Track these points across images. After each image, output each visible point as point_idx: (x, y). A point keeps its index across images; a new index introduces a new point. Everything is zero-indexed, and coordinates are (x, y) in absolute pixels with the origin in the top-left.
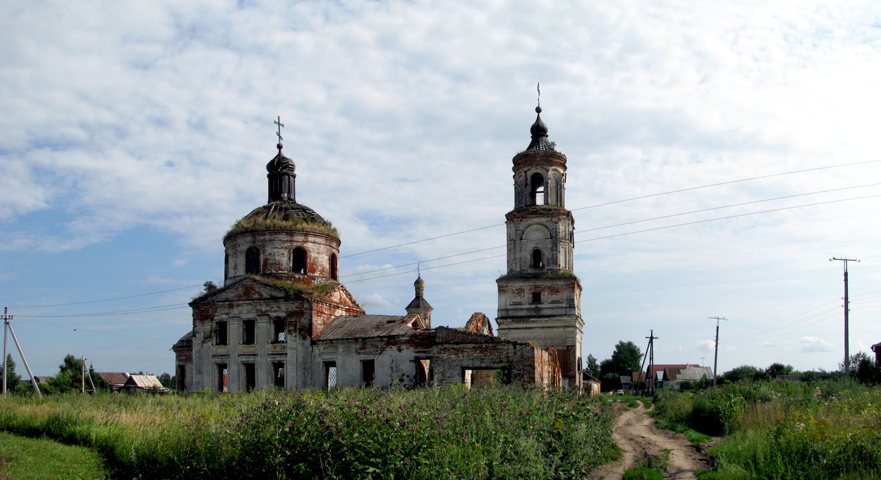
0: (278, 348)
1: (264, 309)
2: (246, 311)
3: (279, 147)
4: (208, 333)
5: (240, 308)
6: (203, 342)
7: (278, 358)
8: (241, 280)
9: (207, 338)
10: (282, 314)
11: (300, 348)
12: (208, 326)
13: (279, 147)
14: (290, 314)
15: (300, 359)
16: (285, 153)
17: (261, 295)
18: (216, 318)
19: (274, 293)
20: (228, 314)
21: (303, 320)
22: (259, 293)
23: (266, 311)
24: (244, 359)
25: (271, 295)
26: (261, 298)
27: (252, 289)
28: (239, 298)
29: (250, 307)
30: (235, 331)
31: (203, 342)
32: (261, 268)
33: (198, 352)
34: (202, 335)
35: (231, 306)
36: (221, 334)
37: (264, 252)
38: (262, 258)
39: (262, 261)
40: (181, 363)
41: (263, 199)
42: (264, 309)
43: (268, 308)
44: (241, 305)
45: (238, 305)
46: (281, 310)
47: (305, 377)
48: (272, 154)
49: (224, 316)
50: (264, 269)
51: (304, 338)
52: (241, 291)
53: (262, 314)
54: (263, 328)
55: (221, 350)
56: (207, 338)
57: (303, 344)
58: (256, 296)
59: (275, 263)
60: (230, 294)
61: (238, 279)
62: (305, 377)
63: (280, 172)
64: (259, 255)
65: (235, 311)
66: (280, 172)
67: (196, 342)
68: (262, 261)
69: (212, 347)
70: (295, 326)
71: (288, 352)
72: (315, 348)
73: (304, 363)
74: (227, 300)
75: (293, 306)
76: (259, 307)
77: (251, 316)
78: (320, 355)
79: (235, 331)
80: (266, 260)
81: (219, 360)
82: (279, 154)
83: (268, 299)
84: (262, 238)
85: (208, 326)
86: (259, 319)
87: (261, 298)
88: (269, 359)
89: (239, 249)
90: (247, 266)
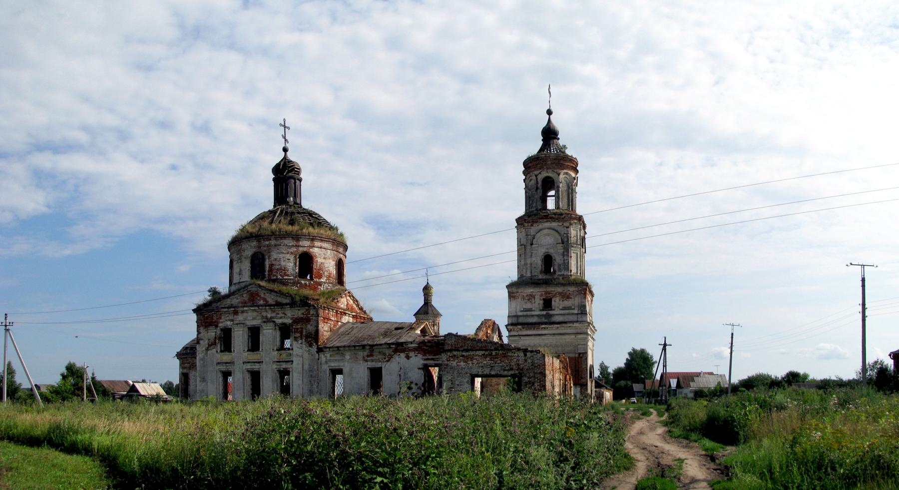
0: (284, 355)
1: (269, 316)
2: (251, 318)
3: (285, 150)
4: (212, 340)
5: (245, 314)
6: (207, 349)
7: (284, 366)
8: (246, 286)
9: (212, 345)
10: (288, 321)
11: (306, 355)
12: (212, 333)
13: (285, 150)
14: (296, 321)
15: (306, 367)
16: (291, 156)
17: (267, 301)
18: (220, 325)
19: (280, 300)
20: (232, 320)
21: (309, 326)
22: (265, 300)
23: (271, 318)
24: (249, 366)
25: (276, 301)
26: (267, 305)
27: (257, 295)
28: (244, 304)
29: (255, 314)
30: (240, 338)
31: (207, 349)
32: (267, 273)
33: (203, 359)
34: (207, 342)
35: (236, 313)
36: (225, 341)
37: (269, 257)
38: (267, 263)
39: (267, 266)
40: (185, 371)
41: (268, 203)
42: (269, 316)
43: (274, 315)
44: (246, 311)
45: (243, 312)
46: (287, 316)
47: (312, 385)
48: (278, 158)
49: (229, 323)
50: (269, 275)
51: (311, 345)
52: (246, 297)
53: (268, 320)
54: (269, 335)
55: (226, 357)
56: (212, 345)
57: (309, 351)
58: (262, 302)
59: (281, 269)
60: (235, 301)
61: (243, 285)
62: (312, 385)
63: (285, 176)
64: (264, 260)
65: (240, 318)
66: (285, 176)
67: (200, 349)
68: (267, 266)
69: (216, 355)
70: (301, 332)
71: (294, 359)
72: (322, 355)
73: (310, 371)
74: (231, 306)
75: (299, 313)
76: (264, 314)
77: (256, 323)
78: (326, 362)
79: (240, 338)
80: (271, 265)
81: (223, 368)
82: (285, 158)
83: (274, 305)
84: (267, 243)
85: (212, 333)
86: (264, 326)
87: (267, 305)
88: (275, 366)
89: (244, 254)
90: (252, 271)
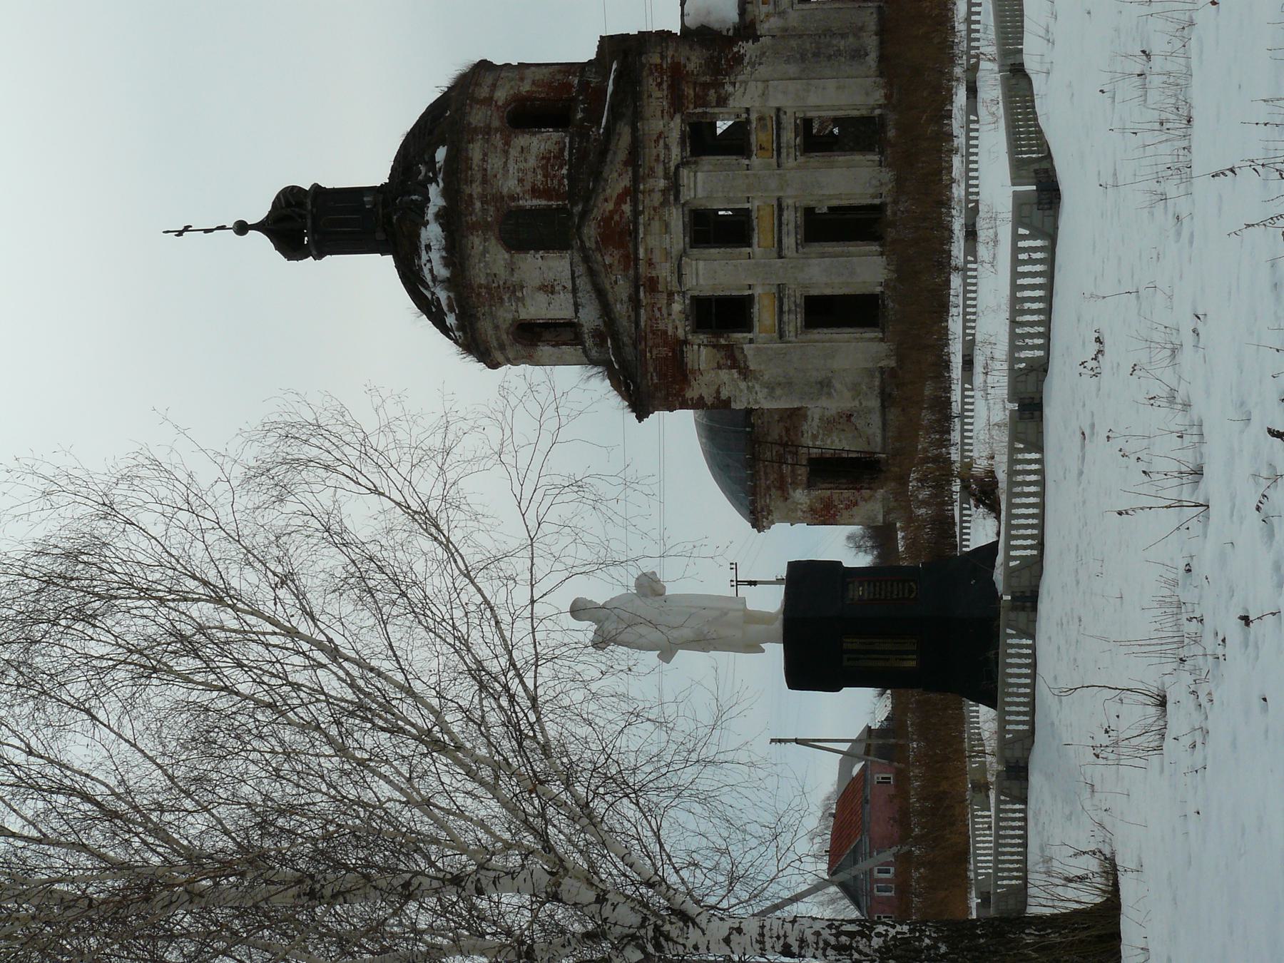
0: (757, 137)
1: (662, 183)
2: (664, 237)
3: (242, 228)
4: (720, 356)
5: (657, 257)
6: (745, 373)
7: (788, 136)
8: (586, 259)
9: (733, 359)
10: (676, 127)
11: (762, 71)
12: (701, 355)
13: (242, 228)
14: (677, 103)
15: (793, 69)
16: (259, 210)
17: (626, 192)
18: (681, 333)
19: (622, 155)
20: (670, 295)
21: (691, 67)
22: (621, 199)
23: (666, 177)
24: (789, 241)
25: (626, 164)
26: (632, 193)
27: (607, 220)
28: (630, 260)
29: (656, 225)
30: (714, 273)
31: (745, 373)
32: (554, 203)
33: (771, 388)
34: (724, 375)
35: (652, 285)
36: (724, 315)
37: (513, 198)
38: (530, 203)
39: (536, 202)
40: (803, 472)
41: (378, 270)
42: (662, 183)
43: (660, 170)
44: (649, 251)
45: (650, 264)
46: (664, 130)
47: (839, 53)
48: (259, 241)
49: (677, 307)
50: (558, 197)
51: (739, 59)
52: (611, 257)
53: (674, 186)
54: (710, 185)
55: (764, 314)
56: (733, 359)
57: (753, 65)
58: (627, 208)
59: (544, 168)
60: (620, 289)
61: (583, 283)
62: (839, 53)
63: (308, 223)
64: (522, 210)
65: (664, 271)
66: (308, 223)
67: (744, 396)
68: (536, 202)
69: (756, 344)
70: (706, 86)
71: (774, 103)
72: (762, 29)
73: (803, 58)
74: (635, 302)
75: (656, 97)
76: (657, 198)
77: (676, 218)
78: (781, 14)
79: (714, 273)
80: (535, 192)
81: (794, 321)
82: (258, 227)
83: (635, 173)
84: (478, 205)
85: (701, 355)
86: (686, 195)
87: (632, 193)
88: (791, 163)
89: (502, 273)
90: (547, 248)
